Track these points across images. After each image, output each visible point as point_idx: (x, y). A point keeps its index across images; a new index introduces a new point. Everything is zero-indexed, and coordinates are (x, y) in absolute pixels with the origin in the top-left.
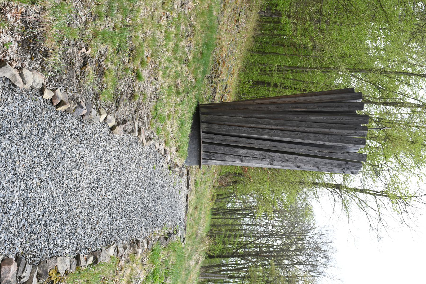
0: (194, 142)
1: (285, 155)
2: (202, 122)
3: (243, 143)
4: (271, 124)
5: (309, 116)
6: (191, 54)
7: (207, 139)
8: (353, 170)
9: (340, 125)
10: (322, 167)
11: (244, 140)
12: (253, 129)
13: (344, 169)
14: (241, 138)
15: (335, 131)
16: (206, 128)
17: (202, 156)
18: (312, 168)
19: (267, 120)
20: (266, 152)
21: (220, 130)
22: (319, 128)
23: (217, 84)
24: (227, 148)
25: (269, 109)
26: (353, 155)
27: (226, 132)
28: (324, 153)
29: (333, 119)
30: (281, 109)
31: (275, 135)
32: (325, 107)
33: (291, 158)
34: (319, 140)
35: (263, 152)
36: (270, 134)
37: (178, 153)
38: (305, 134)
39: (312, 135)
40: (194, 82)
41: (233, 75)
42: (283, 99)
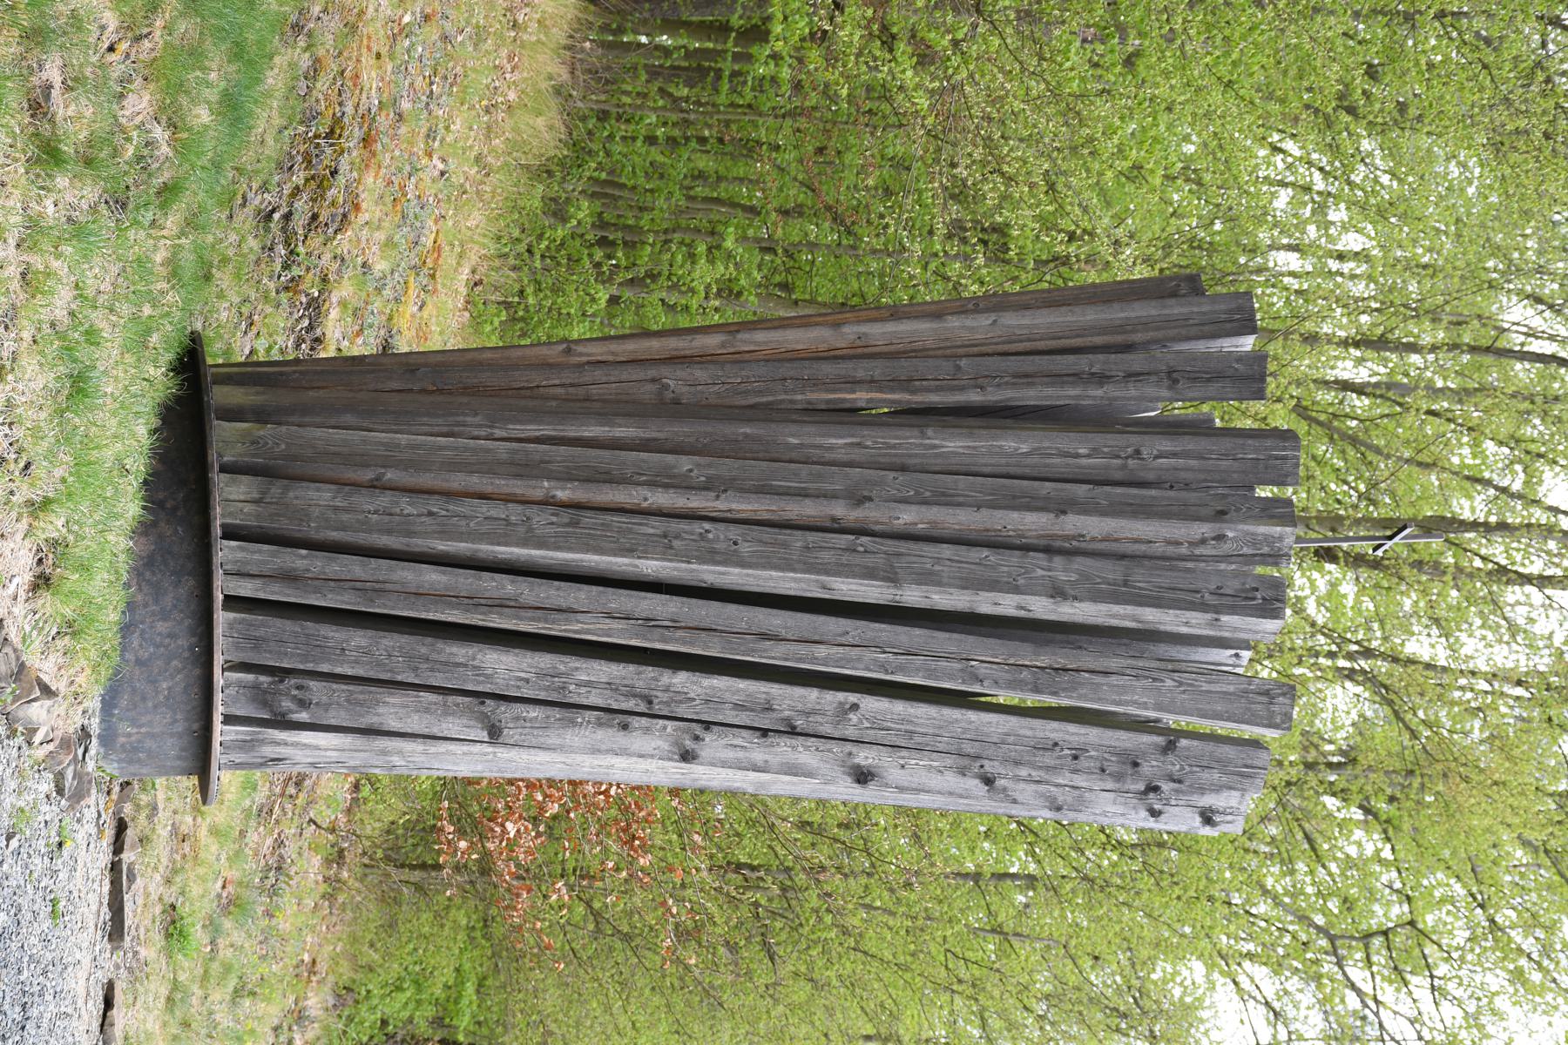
0: (168, 601)
1: (775, 690)
2: (224, 469)
3: (501, 605)
4: (683, 484)
5: (923, 436)
6: (152, 86)
7: (258, 582)
8: (1208, 800)
9: (1119, 490)
10: (1017, 779)
11: (508, 586)
12: (565, 517)
13: (1156, 789)
14: (485, 574)
15: (1093, 526)
16: (248, 508)
17: (218, 697)
18: (951, 780)
19: (656, 457)
20: (650, 672)
21: (345, 517)
22: (993, 506)
23: (325, 280)
24: (391, 642)
25: (669, 395)
26: (1205, 687)
27: (389, 532)
28: (1025, 674)
29: (1077, 456)
30: (746, 392)
31: (713, 552)
32: (1027, 378)
33: (813, 712)
34: (993, 585)
35: (632, 668)
36: (676, 543)
37: (46, 601)
38: (903, 547)
39: (947, 551)
40: (165, 149)
41: (433, 276)
42: (760, 336)
